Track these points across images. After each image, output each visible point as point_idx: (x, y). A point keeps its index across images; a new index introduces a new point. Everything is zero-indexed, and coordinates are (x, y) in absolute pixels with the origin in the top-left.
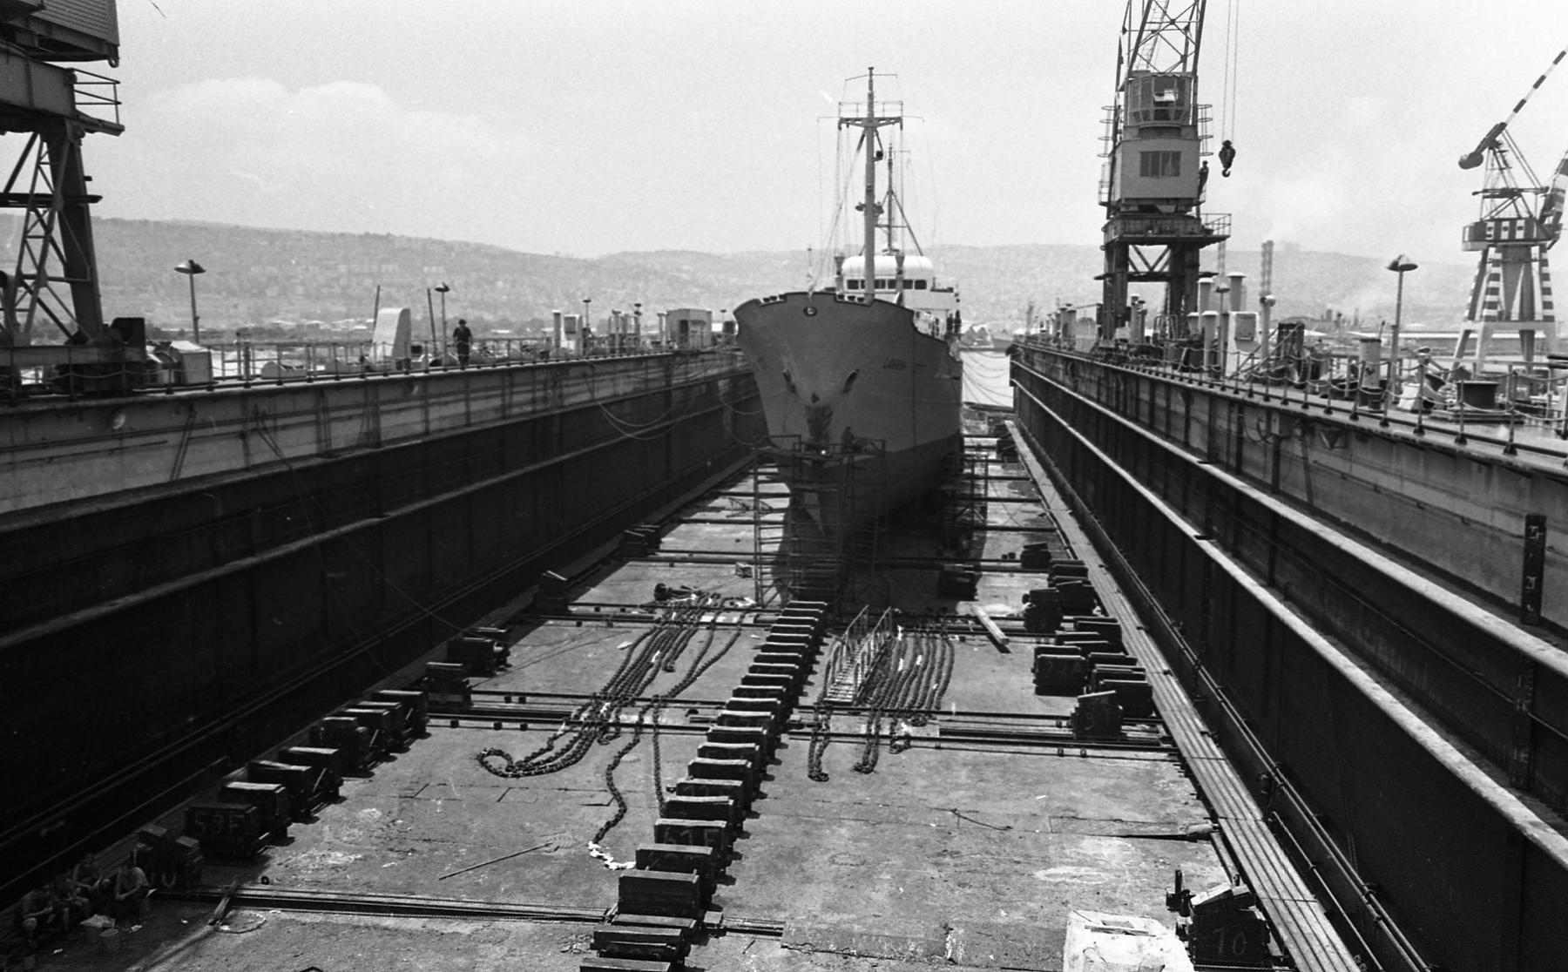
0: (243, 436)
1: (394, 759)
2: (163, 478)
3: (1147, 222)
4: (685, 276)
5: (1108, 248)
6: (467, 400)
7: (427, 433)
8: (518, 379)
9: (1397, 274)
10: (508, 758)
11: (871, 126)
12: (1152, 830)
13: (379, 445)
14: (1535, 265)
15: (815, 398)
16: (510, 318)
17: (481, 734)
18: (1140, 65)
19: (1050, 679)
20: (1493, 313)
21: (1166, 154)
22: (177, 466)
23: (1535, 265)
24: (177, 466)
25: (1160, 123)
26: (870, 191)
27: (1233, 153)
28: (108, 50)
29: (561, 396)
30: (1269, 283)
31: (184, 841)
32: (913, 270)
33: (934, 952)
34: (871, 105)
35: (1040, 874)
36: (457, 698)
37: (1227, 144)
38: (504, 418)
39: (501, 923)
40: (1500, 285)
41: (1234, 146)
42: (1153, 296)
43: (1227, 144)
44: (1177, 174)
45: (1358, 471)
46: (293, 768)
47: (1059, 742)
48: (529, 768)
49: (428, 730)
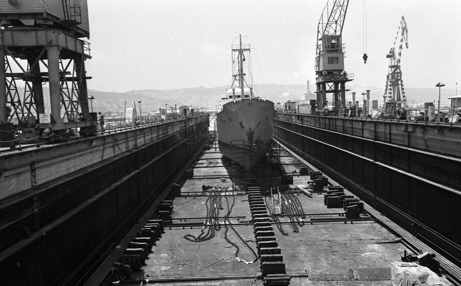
0: (113, 147)
1: (159, 240)
2: (100, 160)
3: (330, 77)
4: (153, 97)
5: (318, 84)
6: (152, 134)
7: (145, 144)
8: (153, 129)
9: (438, 88)
10: (194, 237)
11: (241, 51)
12: (383, 241)
13: (137, 148)
14: (400, 86)
15: (250, 129)
16: (151, 110)
17: (180, 230)
18: (326, 33)
19: (330, 203)
20: (391, 99)
21: (335, 58)
22: (102, 157)
23: (400, 86)
24: (102, 157)
25: (332, 48)
27: (367, 57)
28: (87, 35)
29: (168, 132)
31: (126, 266)
32: (237, 93)
33: (351, 278)
34: (241, 45)
35: (363, 255)
36: (169, 221)
37: (365, 55)
38: (158, 139)
39: (226, 281)
40: (392, 91)
41: (367, 55)
42: (330, 97)
43: (365, 55)
44: (338, 63)
45: (447, 139)
46: (141, 243)
47: (345, 221)
48: (200, 239)
49: (164, 231)
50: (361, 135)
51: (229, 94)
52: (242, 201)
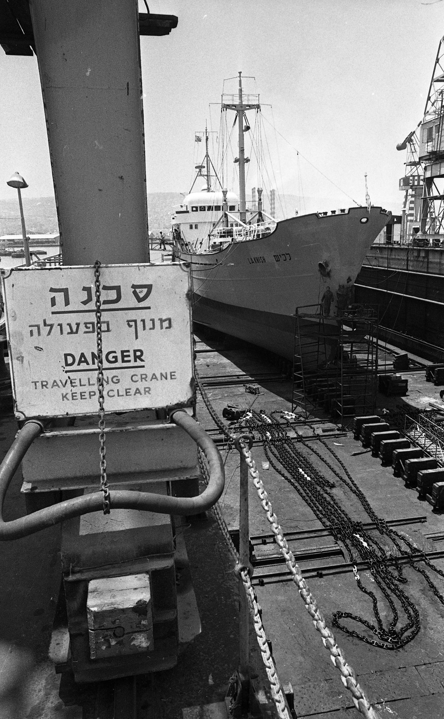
26: (242, 151)
30: (274, 208)
50: (405, 268)
51: (191, 202)
52: (355, 455)
